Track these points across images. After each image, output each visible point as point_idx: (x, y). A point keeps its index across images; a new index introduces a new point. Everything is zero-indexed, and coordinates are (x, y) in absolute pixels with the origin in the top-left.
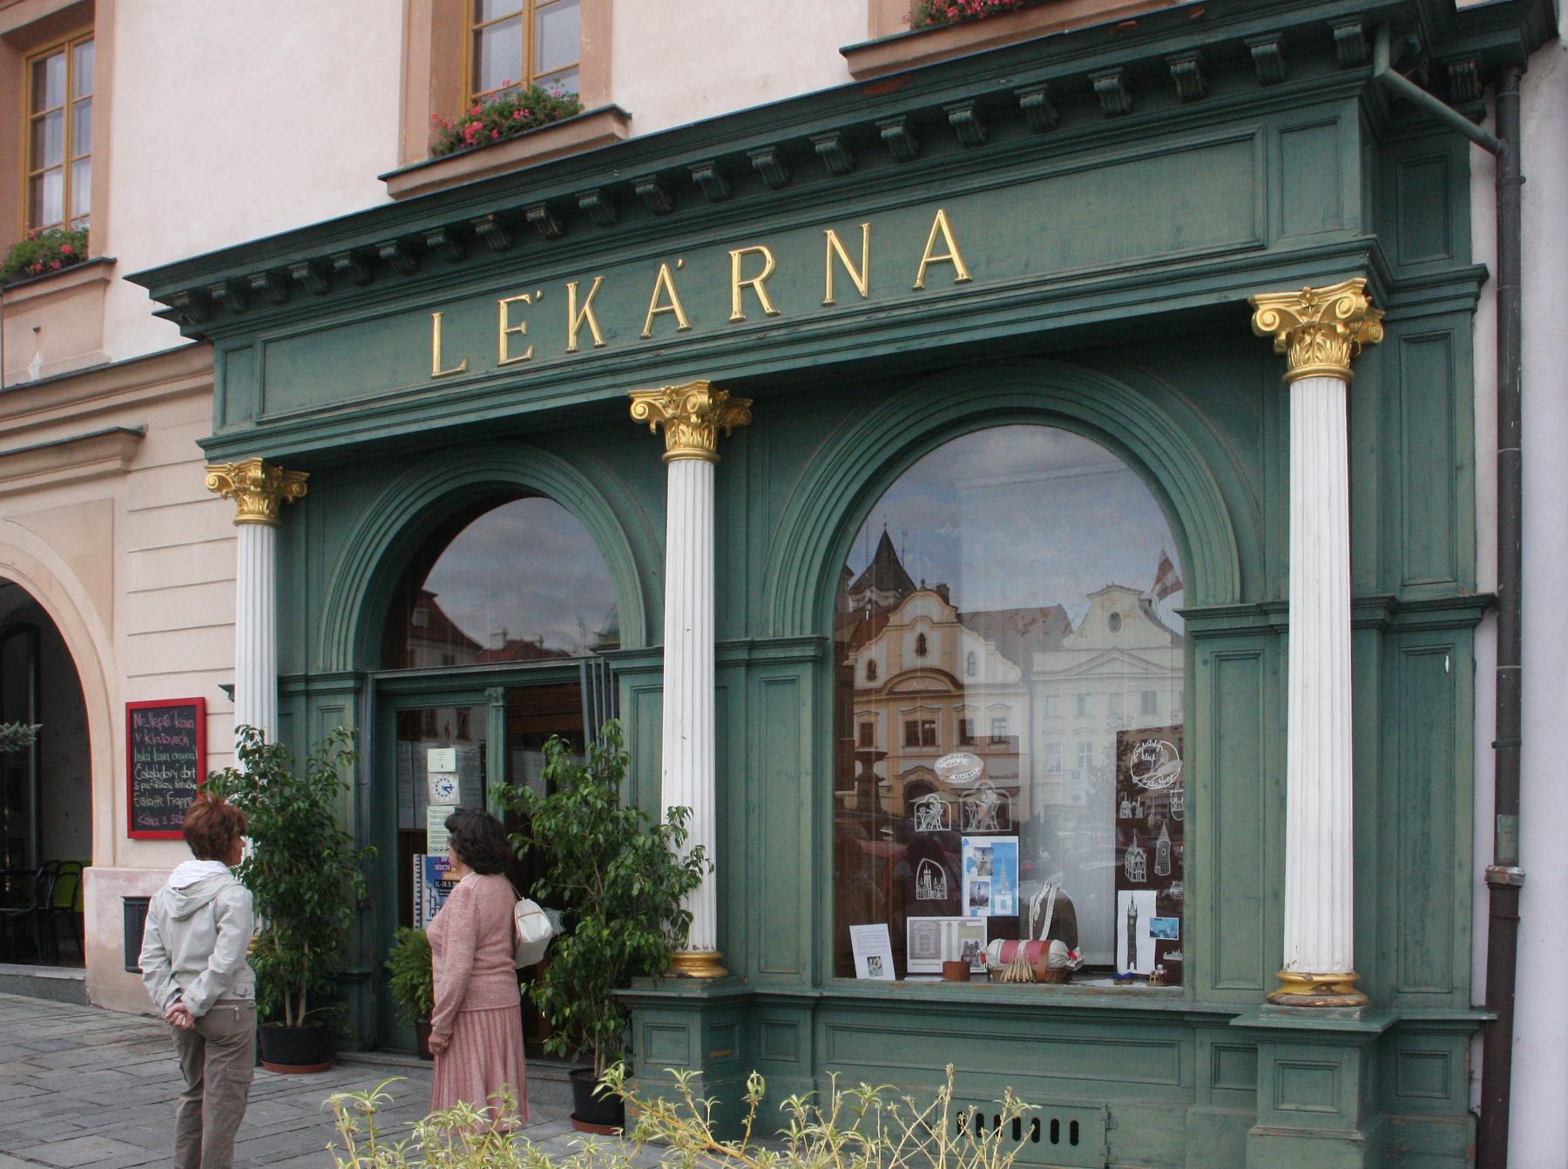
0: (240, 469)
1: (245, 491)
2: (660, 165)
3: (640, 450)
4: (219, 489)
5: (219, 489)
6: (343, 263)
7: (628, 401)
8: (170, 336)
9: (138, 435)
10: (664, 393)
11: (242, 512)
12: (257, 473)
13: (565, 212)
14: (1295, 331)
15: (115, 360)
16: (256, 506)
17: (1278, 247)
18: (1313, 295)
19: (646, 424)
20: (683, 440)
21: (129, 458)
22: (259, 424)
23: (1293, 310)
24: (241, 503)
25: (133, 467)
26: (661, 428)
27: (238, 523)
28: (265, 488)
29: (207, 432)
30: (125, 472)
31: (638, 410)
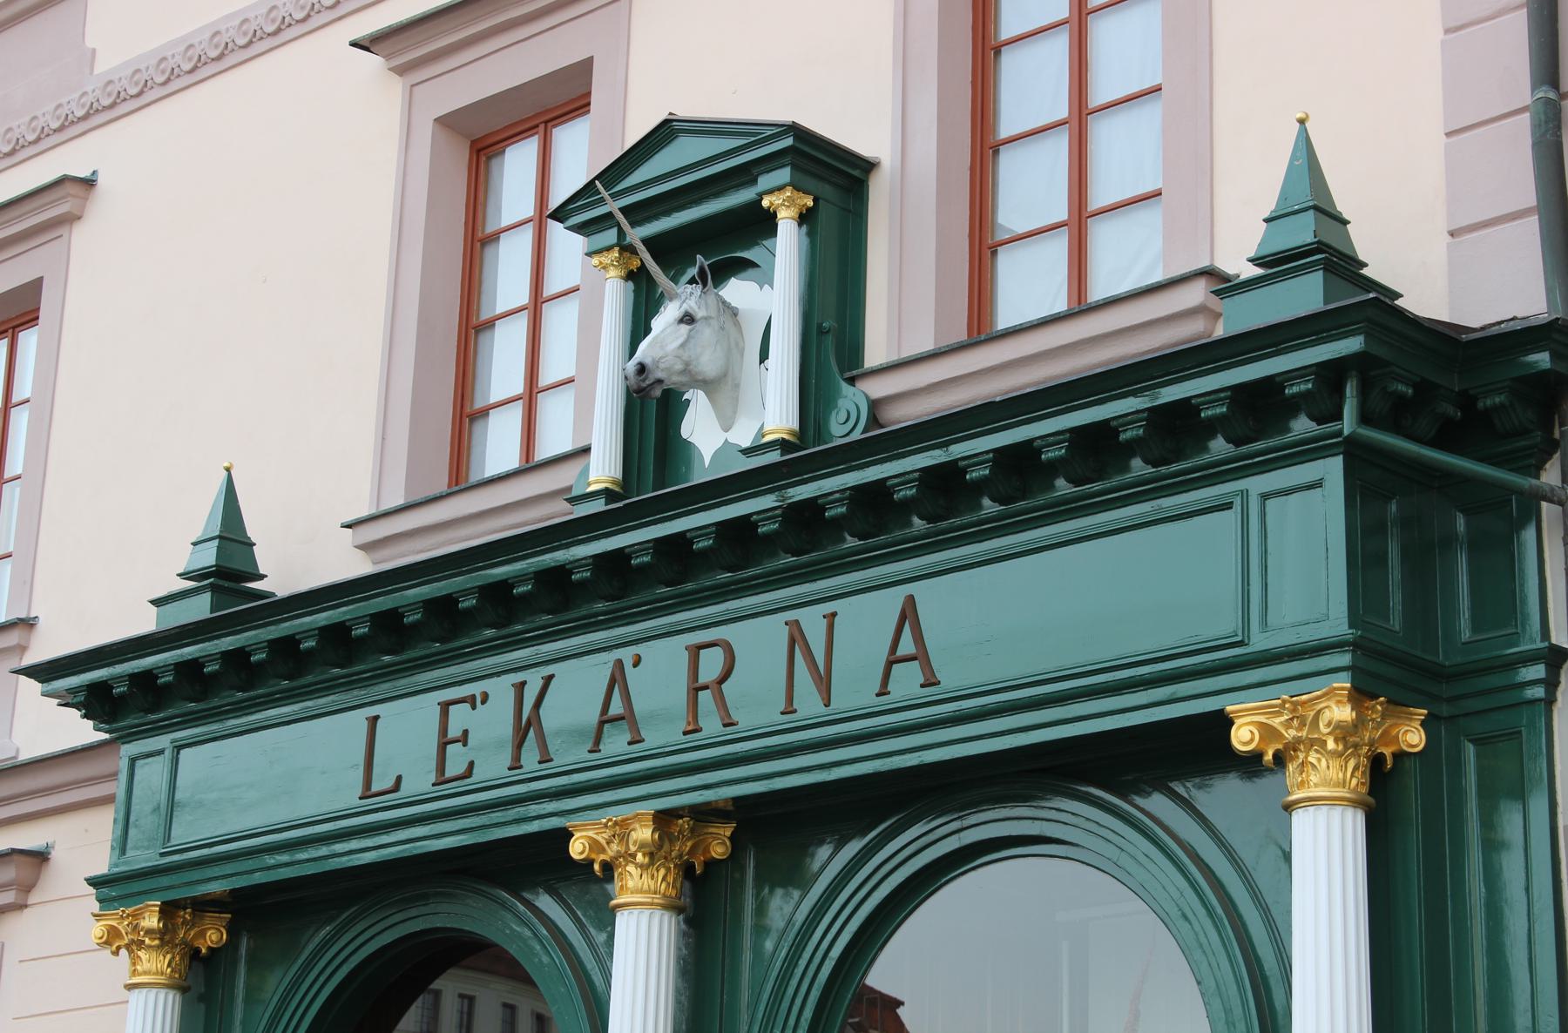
0: (135, 916)
1: (140, 944)
2: (323, 618)
3: (590, 886)
4: (108, 943)
5: (108, 943)
6: (468, 603)
7: (565, 835)
8: (80, 730)
9: (40, 857)
10: (606, 826)
11: (134, 973)
12: (152, 921)
13: (1177, 429)
14: (1287, 746)
15: (24, 756)
16: (154, 963)
17: (1260, 642)
18: (1295, 704)
19: (589, 863)
20: (631, 884)
21: (27, 888)
22: (163, 855)
23: (1276, 722)
24: (135, 960)
25: (32, 899)
26: (608, 868)
27: (131, 987)
28: (165, 937)
29: (102, 868)
30: (22, 906)
31: (577, 849)
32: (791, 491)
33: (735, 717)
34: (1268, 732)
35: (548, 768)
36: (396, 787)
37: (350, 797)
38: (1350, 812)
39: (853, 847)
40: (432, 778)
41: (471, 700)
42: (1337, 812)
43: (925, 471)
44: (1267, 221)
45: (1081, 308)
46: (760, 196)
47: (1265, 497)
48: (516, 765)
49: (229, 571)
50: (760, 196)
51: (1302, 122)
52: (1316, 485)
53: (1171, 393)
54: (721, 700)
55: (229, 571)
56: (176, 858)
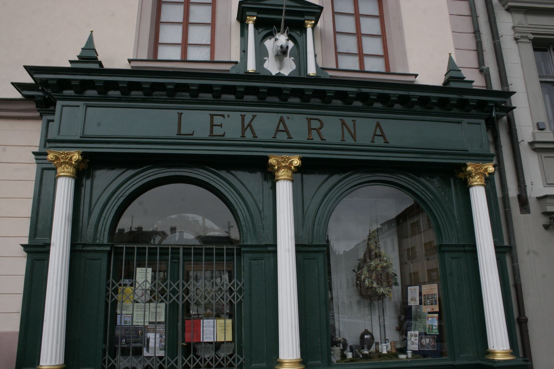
13: (384, 99)
32: (362, 89)
33: (388, 140)
34: (57, 158)
35: (343, 142)
36: (223, 136)
37: (174, 134)
38: (70, 179)
39: (130, 173)
40: (177, 133)
41: (223, 116)
42: (68, 179)
43: (400, 95)
44: (82, 49)
45: (184, 60)
46: (305, 20)
47: (63, 106)
48: (243, 136)
49: (89, 55)
50: (305, 20)
51: (92, 32)
52: (78, 106)
53: (466, 97)
54: (319, 134)
55: (89, 55)
56: (302, 145)
